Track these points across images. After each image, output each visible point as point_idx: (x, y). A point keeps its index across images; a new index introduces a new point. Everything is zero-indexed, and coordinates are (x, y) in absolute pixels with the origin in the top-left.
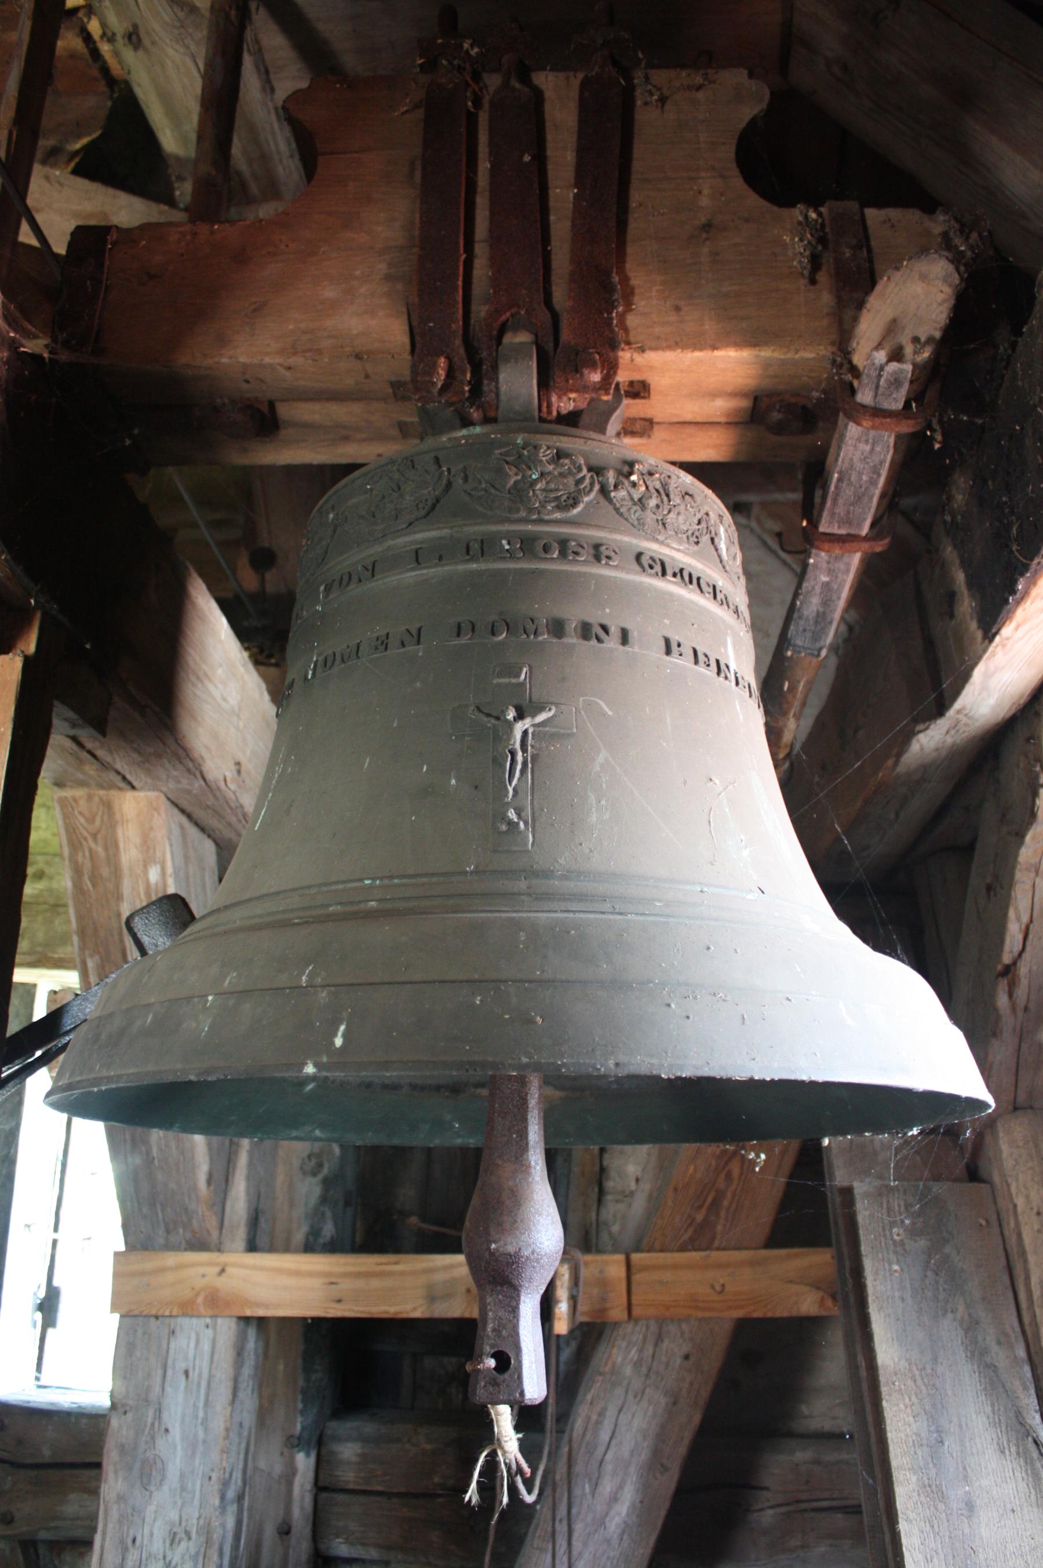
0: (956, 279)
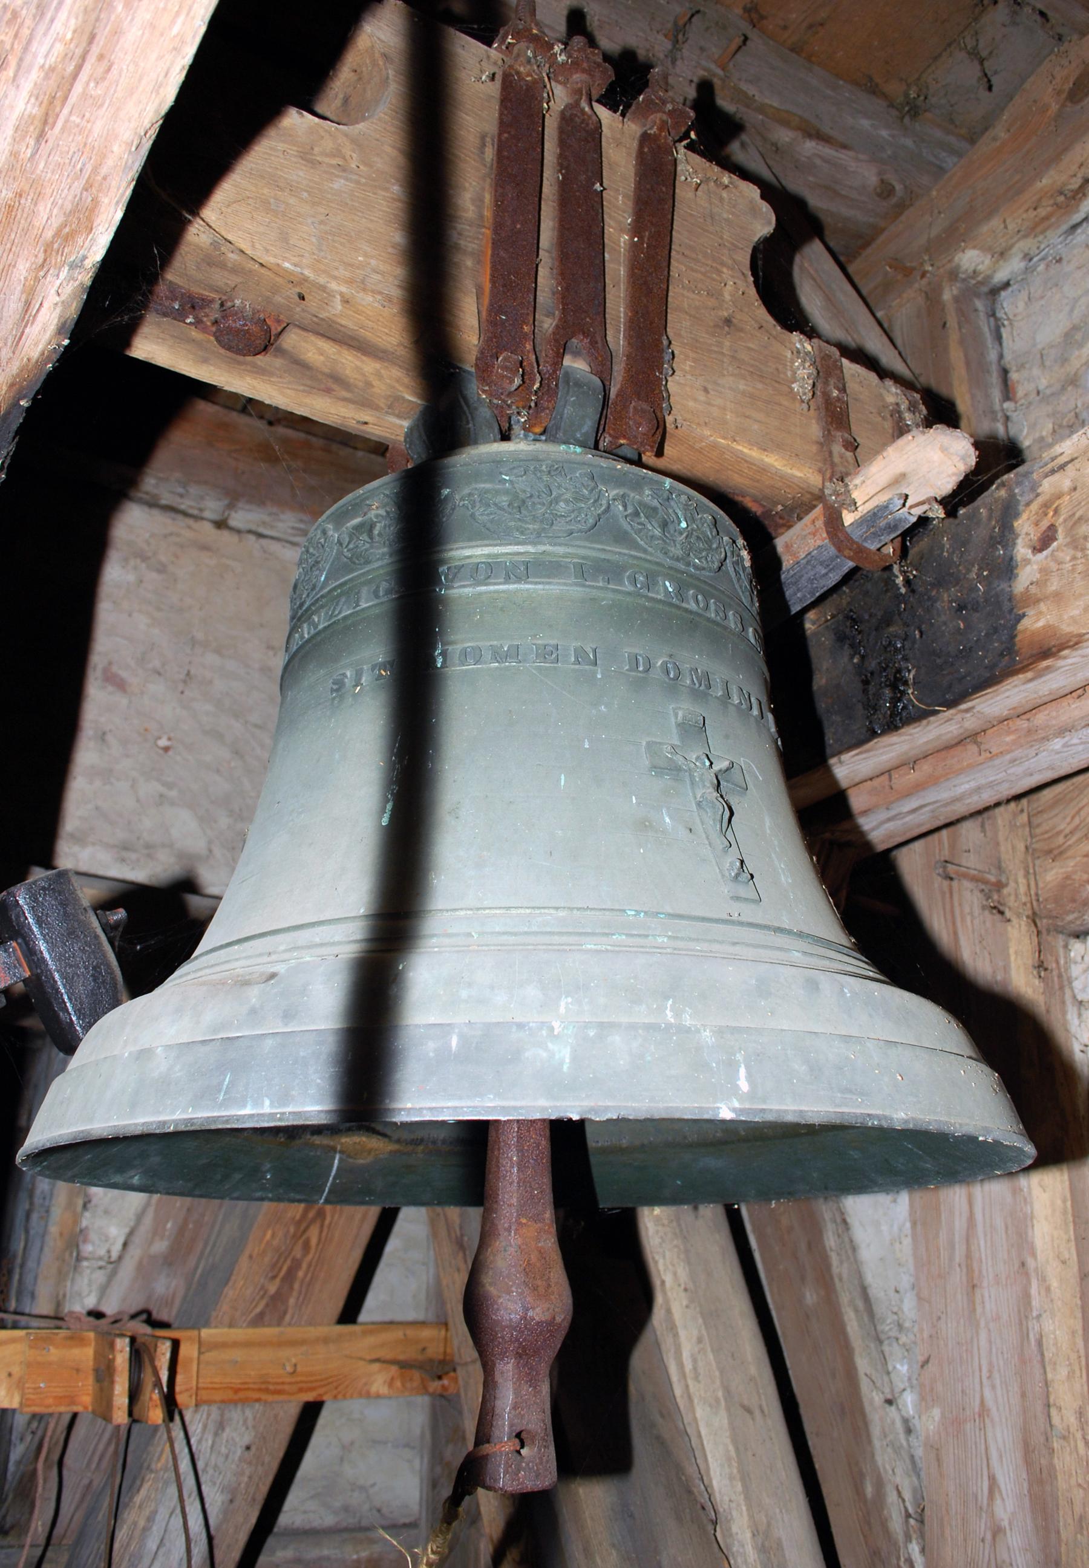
0: (424, 456)
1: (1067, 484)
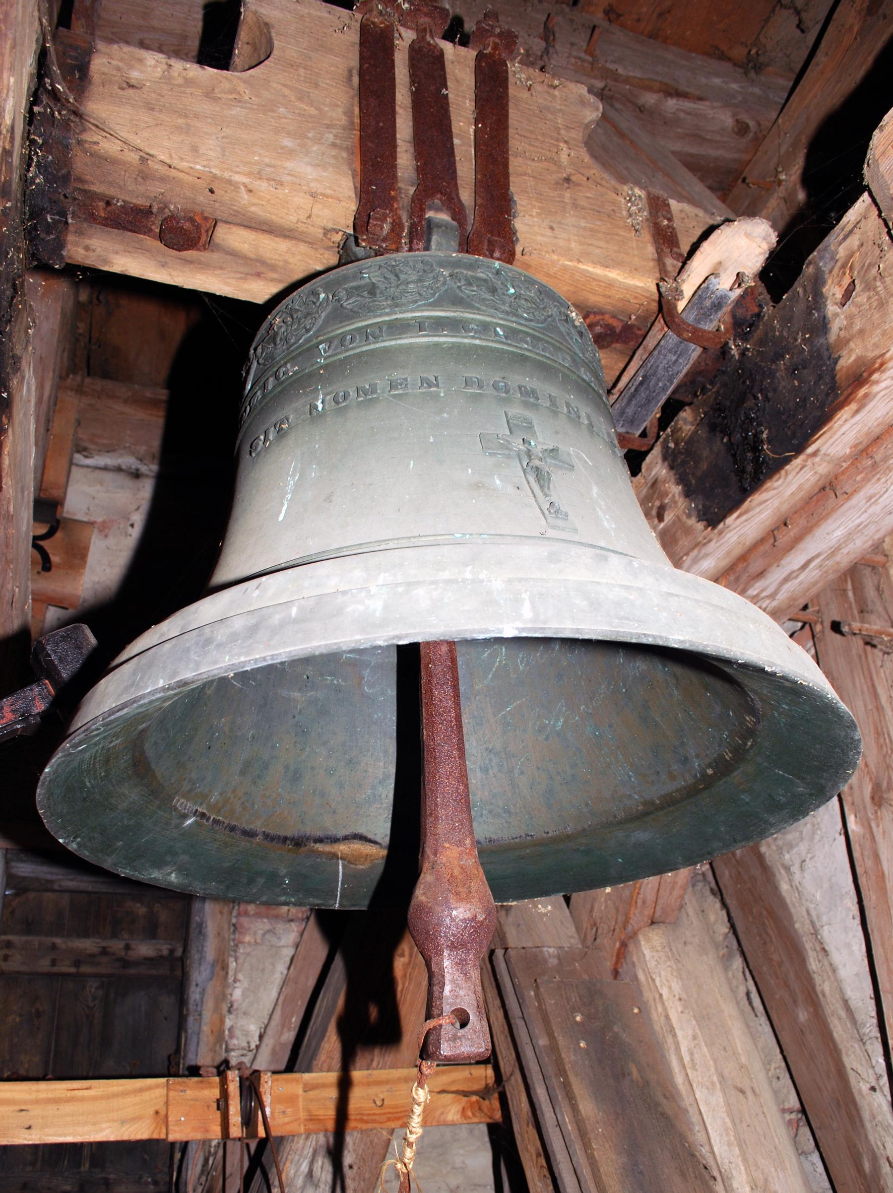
1: (856, 243)
